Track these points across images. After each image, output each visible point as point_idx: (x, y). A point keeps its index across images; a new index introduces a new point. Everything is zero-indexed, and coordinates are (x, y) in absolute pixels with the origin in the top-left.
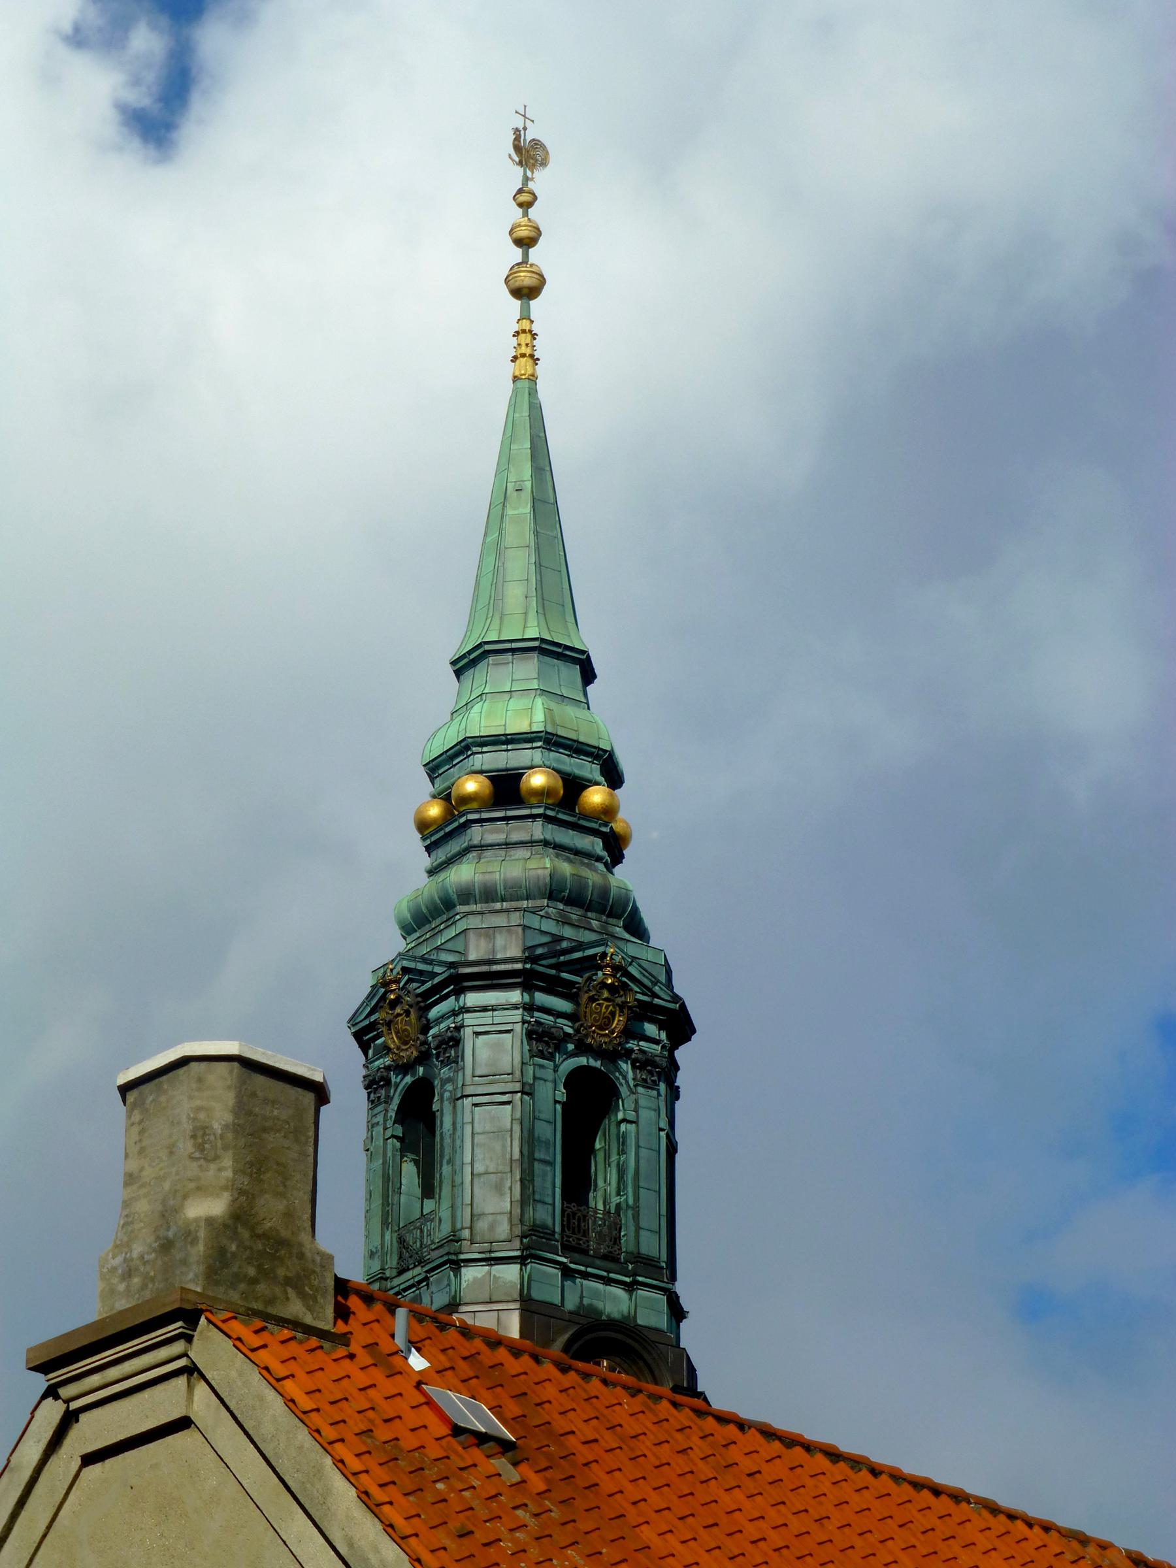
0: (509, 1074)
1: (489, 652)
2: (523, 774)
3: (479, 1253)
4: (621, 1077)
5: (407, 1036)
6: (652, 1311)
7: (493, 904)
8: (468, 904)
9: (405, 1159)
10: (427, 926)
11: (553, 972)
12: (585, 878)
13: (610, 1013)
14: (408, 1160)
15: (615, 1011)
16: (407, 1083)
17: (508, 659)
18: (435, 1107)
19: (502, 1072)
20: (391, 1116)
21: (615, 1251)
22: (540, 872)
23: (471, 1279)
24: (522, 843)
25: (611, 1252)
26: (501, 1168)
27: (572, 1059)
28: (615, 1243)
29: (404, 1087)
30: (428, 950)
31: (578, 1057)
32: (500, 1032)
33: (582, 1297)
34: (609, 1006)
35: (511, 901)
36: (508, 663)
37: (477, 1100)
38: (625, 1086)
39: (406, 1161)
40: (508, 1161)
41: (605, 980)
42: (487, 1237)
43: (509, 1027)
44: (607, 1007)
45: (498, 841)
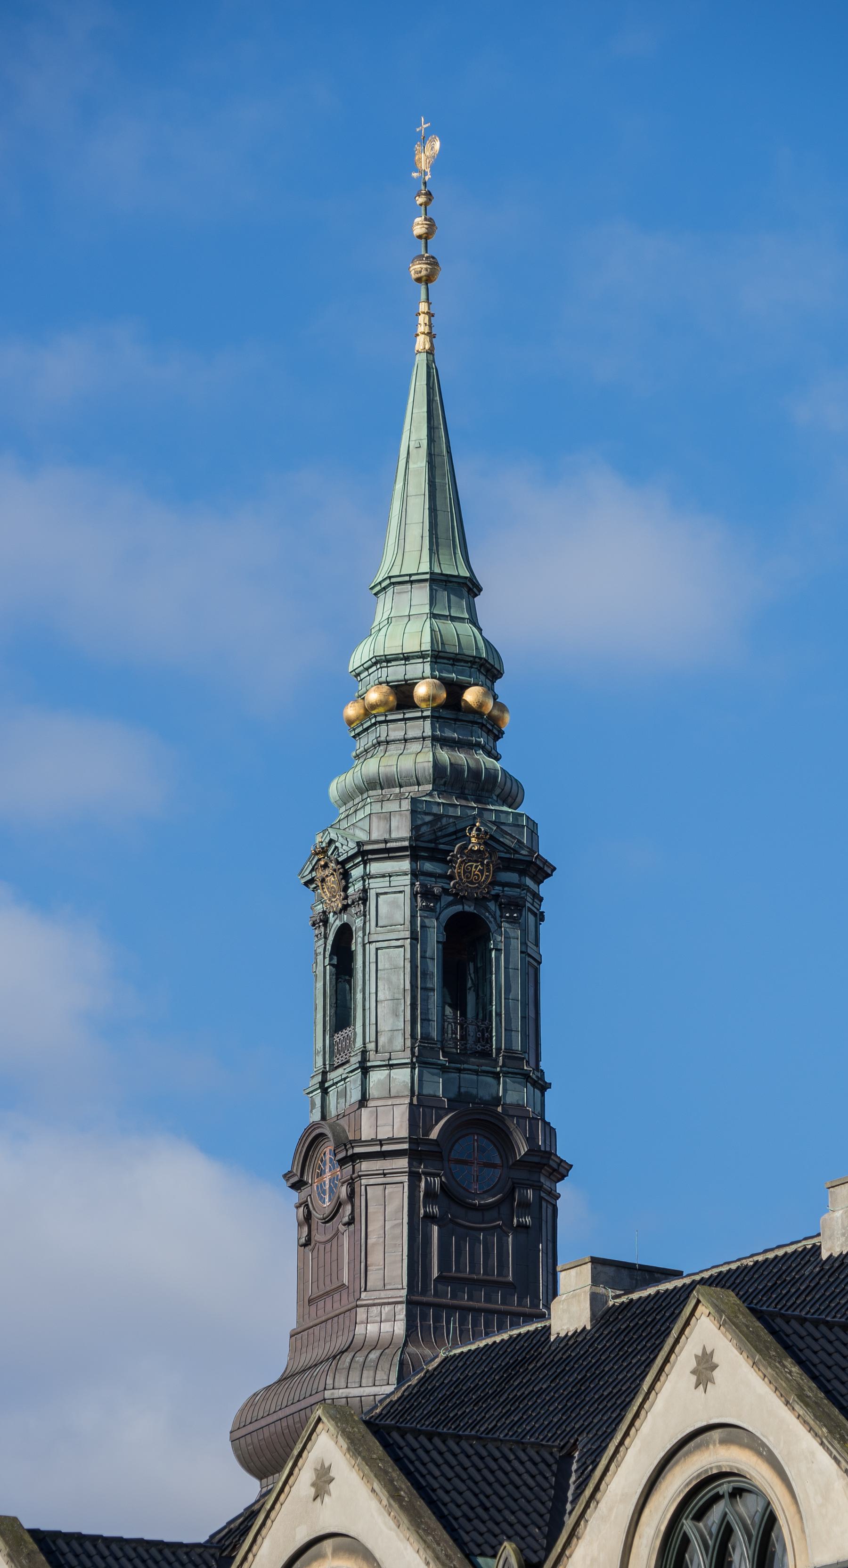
0: (401, 925)
1: (394, 583)
2: (416, 683)
3: (381, 1061)
4: (490, 916)
5: (334, 892)
6: (514, 1092)
7: (394, 789)
8: (375, 789)
9: (340, 980)
10: (351, 802)
11: (433, 845)
12: (461, 765)
13: (478, 871)
14: (342, 980)
15: (483, 869)
16: (337, 925)
17: (408, 588)
18: (353, 948)
19: (397, 923)
20: (328, 949)
21: (487, 1048)
22: (426, 764)
23: (376, 1081)
24: (415, 738)
25: (484, 1050)
26: (397, 996)
27: (451, 908)
28: (487, 1043)
29: (335, 928)
30: (349, 825)
31: (456, 906)
32: (395, 892)
33: (460, 1087)
34: (478, 866)
35: (406, 786)
36: (408, 592)
37: (379, 945)
38: (493, 922)
39: (341, 982)
40: (402, 991)
41: (473, 848)
42: (387, 1048)
43: (401, 889)
44: (476, 867)
45: (398, 737)
